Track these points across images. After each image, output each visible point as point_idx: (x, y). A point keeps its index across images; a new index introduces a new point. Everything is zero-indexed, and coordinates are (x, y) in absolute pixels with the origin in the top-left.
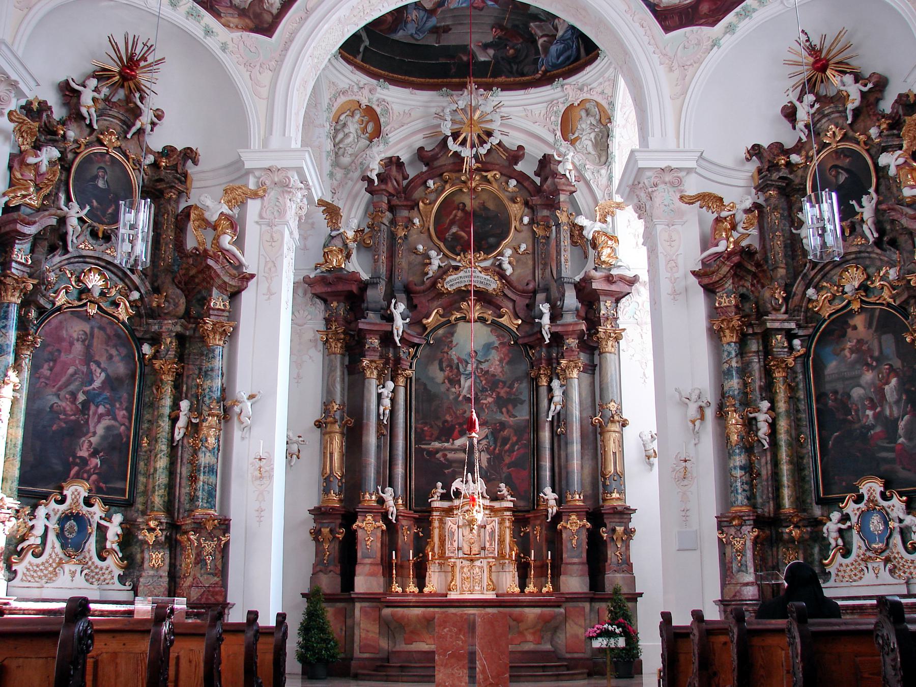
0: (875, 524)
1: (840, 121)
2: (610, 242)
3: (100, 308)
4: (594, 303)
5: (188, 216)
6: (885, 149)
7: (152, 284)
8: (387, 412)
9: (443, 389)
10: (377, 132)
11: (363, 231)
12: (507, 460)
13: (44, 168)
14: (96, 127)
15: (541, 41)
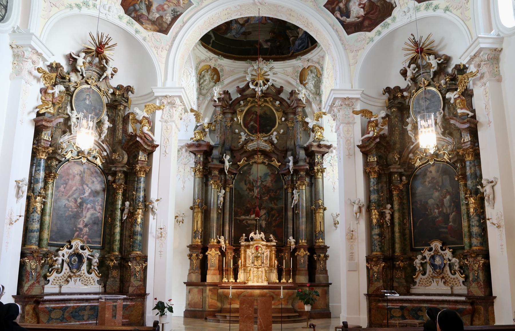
0: (438, 261)
1: (427, 77)
2: (320, 130)
3: (88, 160)
4: (313, 154)
5: (129, 117)
6: (448, 91)
7: (112, 148)
8: (222, 203)
9: (246, 193)
10: (218, 80)
11: (211, 123)
12: (274, 224)
13: (56, 95)
14: (84, 75)
15: (291, 39)
